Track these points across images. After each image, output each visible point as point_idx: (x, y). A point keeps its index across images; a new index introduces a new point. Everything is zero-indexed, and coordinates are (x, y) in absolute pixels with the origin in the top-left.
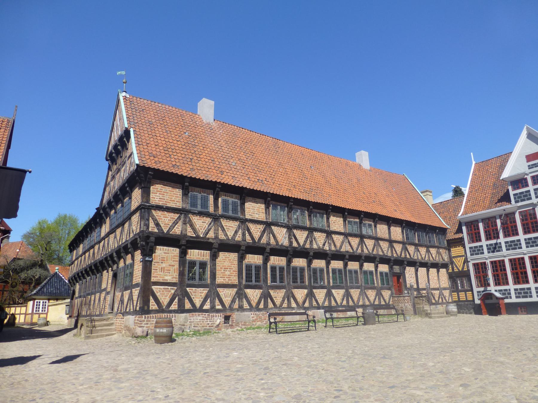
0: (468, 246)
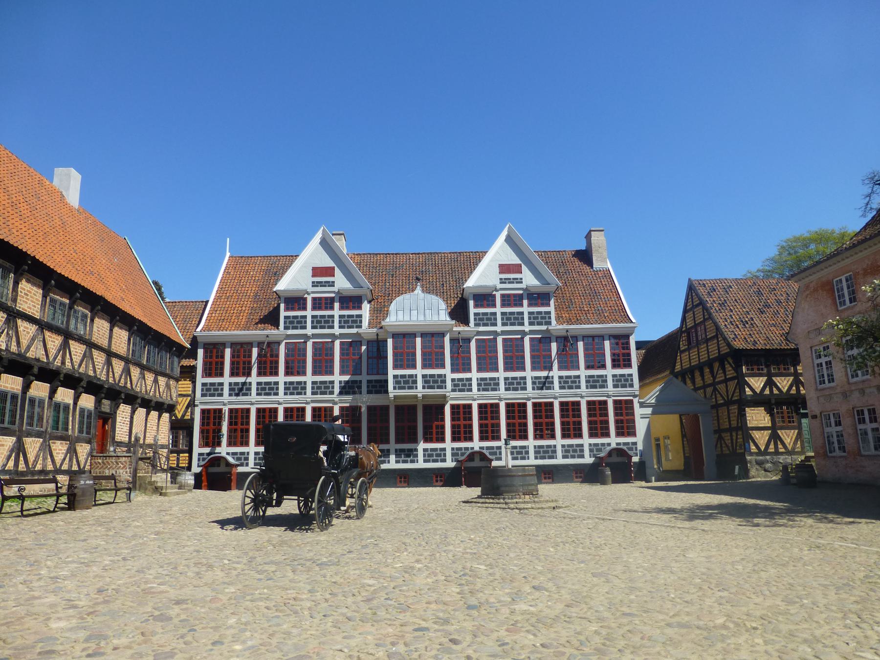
0: (200, 380)
